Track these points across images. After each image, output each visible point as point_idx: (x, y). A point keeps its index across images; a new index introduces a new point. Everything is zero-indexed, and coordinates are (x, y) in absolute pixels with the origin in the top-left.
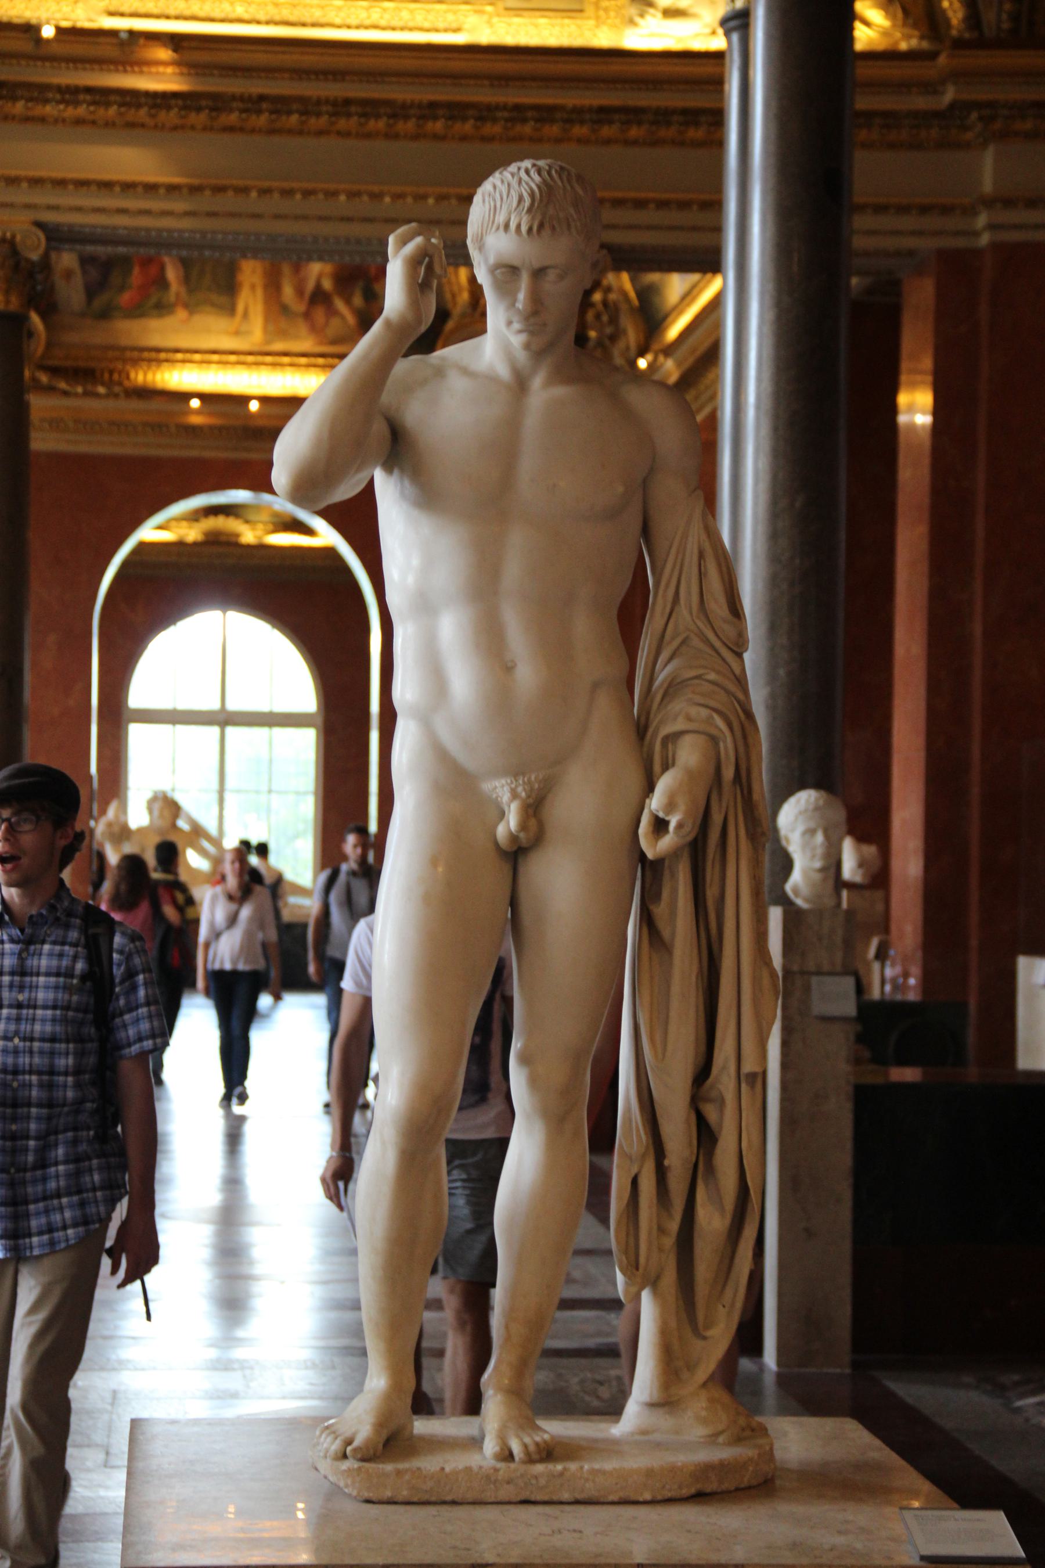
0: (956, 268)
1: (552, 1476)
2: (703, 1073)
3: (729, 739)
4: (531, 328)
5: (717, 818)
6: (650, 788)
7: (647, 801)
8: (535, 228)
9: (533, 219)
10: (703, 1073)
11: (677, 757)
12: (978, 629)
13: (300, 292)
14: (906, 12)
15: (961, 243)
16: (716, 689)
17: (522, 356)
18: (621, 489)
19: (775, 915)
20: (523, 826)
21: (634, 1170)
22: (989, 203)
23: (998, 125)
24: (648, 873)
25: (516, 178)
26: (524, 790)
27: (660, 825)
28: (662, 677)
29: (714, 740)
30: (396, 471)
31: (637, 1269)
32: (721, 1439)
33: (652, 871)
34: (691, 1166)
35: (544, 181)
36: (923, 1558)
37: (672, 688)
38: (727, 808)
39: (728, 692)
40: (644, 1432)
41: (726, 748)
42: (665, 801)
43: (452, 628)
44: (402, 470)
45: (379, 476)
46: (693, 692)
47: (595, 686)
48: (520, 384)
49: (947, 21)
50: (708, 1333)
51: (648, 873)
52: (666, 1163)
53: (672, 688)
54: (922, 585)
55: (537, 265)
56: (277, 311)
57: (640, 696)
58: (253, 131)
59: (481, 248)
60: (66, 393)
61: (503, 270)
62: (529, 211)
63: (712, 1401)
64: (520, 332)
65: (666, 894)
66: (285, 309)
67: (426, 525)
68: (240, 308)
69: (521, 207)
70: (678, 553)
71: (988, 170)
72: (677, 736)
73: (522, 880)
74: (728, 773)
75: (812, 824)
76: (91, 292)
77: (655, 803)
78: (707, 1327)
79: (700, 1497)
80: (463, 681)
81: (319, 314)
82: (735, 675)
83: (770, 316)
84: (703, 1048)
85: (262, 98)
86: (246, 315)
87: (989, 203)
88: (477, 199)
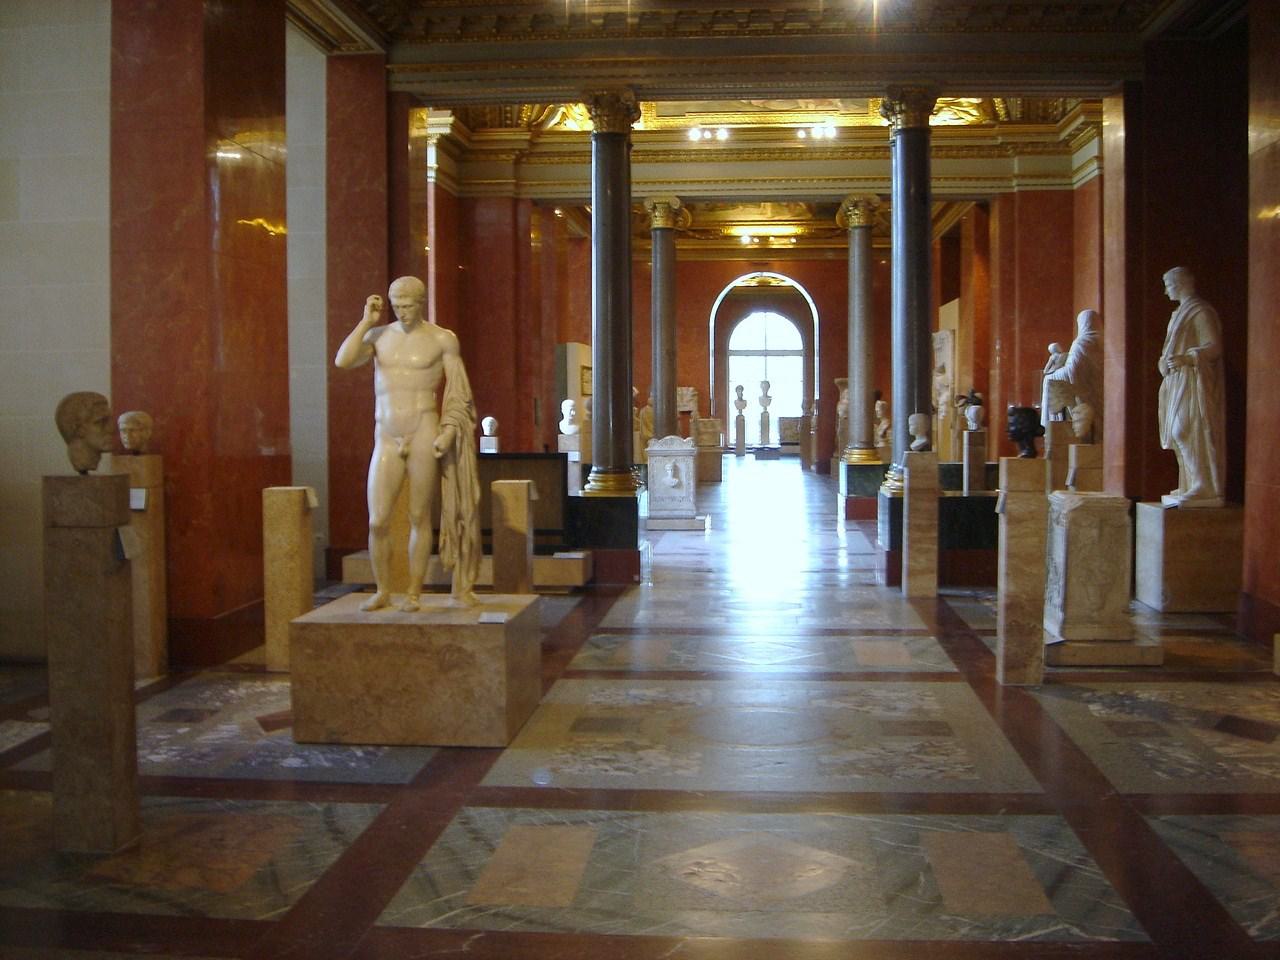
0: (1007, 198)
14: (984, 111)
15: (1007, 191)
22: (1016, 177)
23: (1018, 150)
58: (752, 160)
60: (699, 239)
71: (1016, 164)
85: (755, 149)
87: (1016, 177)
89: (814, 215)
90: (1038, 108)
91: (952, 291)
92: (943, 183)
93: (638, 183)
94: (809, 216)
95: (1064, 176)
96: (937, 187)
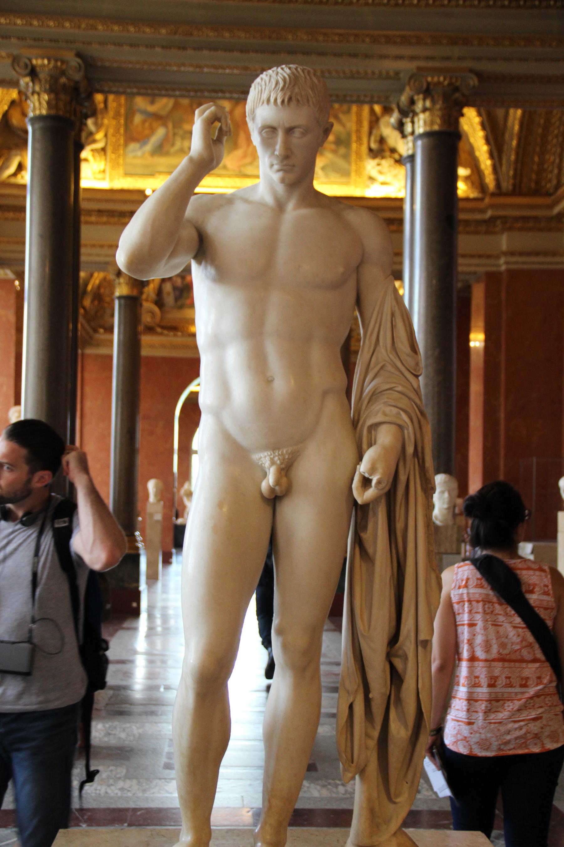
0: (492, 279)
2: (394, 639)
3: (411, 429)
4: (285, 168)
5: (403, 478)
6: (360, 458)
7: (358, 466)
8: (286, 100)
9: (285, 94)
10: (394, 639)
11: (377, 439)
12: (502, 415)
15: (494, 269)
16: (403, 397)
17: (280, 189)
18: (341, 270)
20: (278, 482)
21: (351, 701)
22: (505, 254)
24: (359, 513)
25: (275, 72)
26: (279, 459)
27: (366, 482)
28: (368, 390)
29: (401, 428)
30: (203, 263)
31: (352, 763)
33: (361, 512)
34: (386, 697)
35: (293, 73)
37: (375, 395)
38: (409, 472)
39: (410, 399)
41: (408, 433)
42: (369, 466)
43: (234, 357)
44: (206, 261)
45: (194, 266)
46: (388, 398)
47: (325, 393)
49: (488, 187)
50: (398, 800)
51: (359, 513)
52: (371, 696)
53: (375, 395)
54: (481, 399)
55: (287, 125)
57: (355, 401)
59: (253, 119)
61: (267, 130)
62: (282, 89)
64: (278, 171)
65: (370, 526)
67: (219, 292)
69: (277, 88)
70: (378, 313)
71: (504, 241)
72: (376, 426)
73: (278, 517)
74: (410, 450)
75: (443, 489)
76: (177, 299)
77: (363, 468)
78: (397, 796)
80: (241, 389)
82: (414, 389)
83: (424, 274)
84: (394, 623)
87: (505, 254)
88: (252, 90)
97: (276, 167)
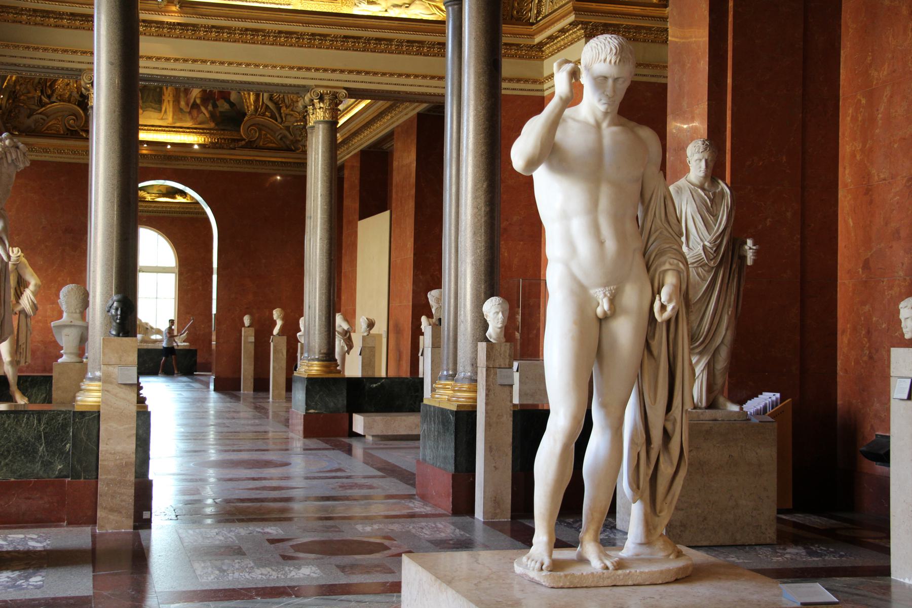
1: (625, 575)
13: (187, 104)
19: (482, 346)
32: (671, 557)
36: (802, 604)
40: (638, 555)
48: (598, 126)
56: (178, 110)
63: (664, 541)
66: (181, 110)
68: (163, 109)
72: (665, 271)
73: (604, 330)
78: (660, 512)
79: (676, 581)
81: (195, 112)
85: (213, 27)
86: (166, 112)
89: (216, 124)
90: (513, 7)
91: (371, 206)
92: (153, 64)
93: (150, 58)
94: (212, 125)
95: (535, 81)
96: (145, 68)
97: (603, 101)
